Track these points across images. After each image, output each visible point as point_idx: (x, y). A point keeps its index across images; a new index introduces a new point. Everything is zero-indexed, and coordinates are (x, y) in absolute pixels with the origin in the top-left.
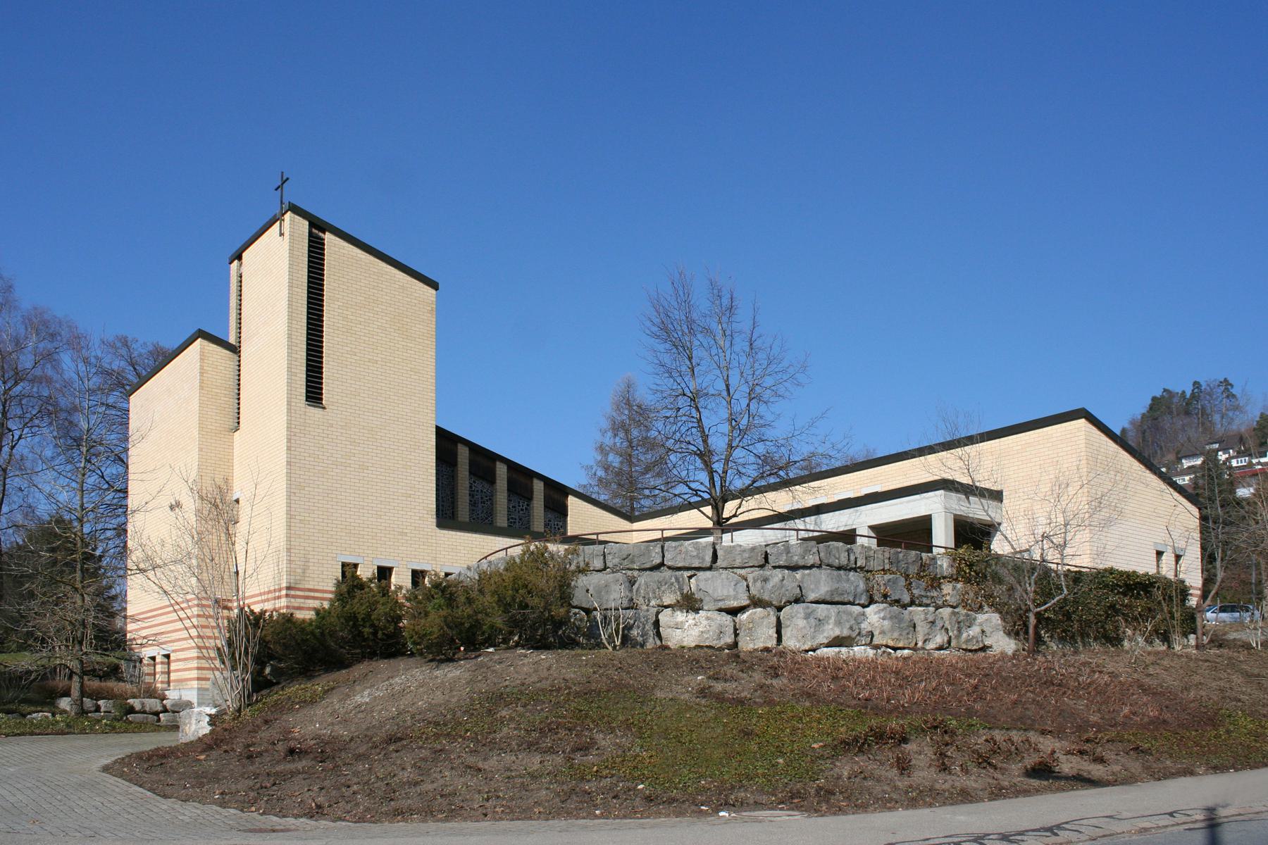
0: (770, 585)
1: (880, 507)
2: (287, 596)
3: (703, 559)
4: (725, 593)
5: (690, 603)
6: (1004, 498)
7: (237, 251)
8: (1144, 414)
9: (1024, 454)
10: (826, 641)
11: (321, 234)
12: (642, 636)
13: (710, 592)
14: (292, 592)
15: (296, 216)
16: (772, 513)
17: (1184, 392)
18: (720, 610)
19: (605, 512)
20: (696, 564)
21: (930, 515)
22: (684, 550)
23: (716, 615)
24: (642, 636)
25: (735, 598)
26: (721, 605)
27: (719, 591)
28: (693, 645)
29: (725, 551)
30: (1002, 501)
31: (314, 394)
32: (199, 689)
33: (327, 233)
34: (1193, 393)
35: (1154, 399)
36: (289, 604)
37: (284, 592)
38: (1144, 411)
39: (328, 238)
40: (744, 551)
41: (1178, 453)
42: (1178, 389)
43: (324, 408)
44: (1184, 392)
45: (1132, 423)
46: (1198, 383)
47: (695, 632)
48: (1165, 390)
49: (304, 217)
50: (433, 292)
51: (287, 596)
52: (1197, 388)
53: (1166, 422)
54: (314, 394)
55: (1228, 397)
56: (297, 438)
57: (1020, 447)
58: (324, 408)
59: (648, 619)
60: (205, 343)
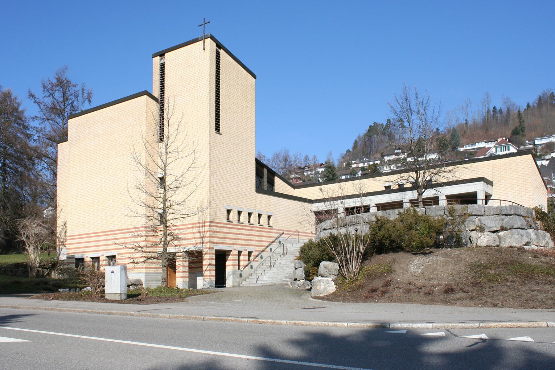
0: (505, 222)
1: (447, 188)
2: (210, 226)
3: (481, 212)
4: (492, 225)
5: (481, 229)
6: (494, 185)
7: (162, 51)
8: (366, 134)
9: (503, 167)
10: (524, 244)
11: (219, 50)
12: (466, 242)
13: (486, 224)
14: (213, 224)
15: (212, 41)
16: (434, 188)
17: (382, 124)
18: (490, 232)
19: (283, 182)
20: (479, 214)
21: (477, 192)
22: (475, 208)
23: (489, 233)
24: (466, 242)
25: (496, 227)
26: (491, 230)
27: (490, 224)
28: (485, 245)
29: (488, 209)
30: (493, 186)
31: (218, 129)
32: (146, 273)
33: (221, 50)
34: (387, 125)
35: (370, 127)
36: (210, 230)
37: (208, 224)
38: (365, 132)
39: (222, 52)
40: (494, 209)
41: (382, 153)
42: (379, 122)
43: (221, 134)
44: (382, 124)
45: (359, 137)
46: (390, 120)
47: (485, 240)
48: (374, 123)
49: (215, 41)
50: (254, 80)
51: (210, 226)
52: (389, 122)
53: (375, 138)
54: (218, 129)
55: (402, 127)
56: (213, 149)
57: (501, 164)
58: (221, 134)
59: (467, 235)
60: (148, 98)
